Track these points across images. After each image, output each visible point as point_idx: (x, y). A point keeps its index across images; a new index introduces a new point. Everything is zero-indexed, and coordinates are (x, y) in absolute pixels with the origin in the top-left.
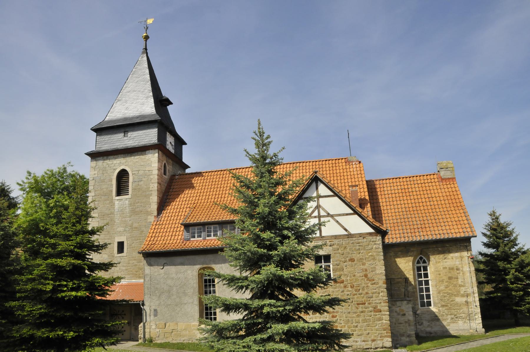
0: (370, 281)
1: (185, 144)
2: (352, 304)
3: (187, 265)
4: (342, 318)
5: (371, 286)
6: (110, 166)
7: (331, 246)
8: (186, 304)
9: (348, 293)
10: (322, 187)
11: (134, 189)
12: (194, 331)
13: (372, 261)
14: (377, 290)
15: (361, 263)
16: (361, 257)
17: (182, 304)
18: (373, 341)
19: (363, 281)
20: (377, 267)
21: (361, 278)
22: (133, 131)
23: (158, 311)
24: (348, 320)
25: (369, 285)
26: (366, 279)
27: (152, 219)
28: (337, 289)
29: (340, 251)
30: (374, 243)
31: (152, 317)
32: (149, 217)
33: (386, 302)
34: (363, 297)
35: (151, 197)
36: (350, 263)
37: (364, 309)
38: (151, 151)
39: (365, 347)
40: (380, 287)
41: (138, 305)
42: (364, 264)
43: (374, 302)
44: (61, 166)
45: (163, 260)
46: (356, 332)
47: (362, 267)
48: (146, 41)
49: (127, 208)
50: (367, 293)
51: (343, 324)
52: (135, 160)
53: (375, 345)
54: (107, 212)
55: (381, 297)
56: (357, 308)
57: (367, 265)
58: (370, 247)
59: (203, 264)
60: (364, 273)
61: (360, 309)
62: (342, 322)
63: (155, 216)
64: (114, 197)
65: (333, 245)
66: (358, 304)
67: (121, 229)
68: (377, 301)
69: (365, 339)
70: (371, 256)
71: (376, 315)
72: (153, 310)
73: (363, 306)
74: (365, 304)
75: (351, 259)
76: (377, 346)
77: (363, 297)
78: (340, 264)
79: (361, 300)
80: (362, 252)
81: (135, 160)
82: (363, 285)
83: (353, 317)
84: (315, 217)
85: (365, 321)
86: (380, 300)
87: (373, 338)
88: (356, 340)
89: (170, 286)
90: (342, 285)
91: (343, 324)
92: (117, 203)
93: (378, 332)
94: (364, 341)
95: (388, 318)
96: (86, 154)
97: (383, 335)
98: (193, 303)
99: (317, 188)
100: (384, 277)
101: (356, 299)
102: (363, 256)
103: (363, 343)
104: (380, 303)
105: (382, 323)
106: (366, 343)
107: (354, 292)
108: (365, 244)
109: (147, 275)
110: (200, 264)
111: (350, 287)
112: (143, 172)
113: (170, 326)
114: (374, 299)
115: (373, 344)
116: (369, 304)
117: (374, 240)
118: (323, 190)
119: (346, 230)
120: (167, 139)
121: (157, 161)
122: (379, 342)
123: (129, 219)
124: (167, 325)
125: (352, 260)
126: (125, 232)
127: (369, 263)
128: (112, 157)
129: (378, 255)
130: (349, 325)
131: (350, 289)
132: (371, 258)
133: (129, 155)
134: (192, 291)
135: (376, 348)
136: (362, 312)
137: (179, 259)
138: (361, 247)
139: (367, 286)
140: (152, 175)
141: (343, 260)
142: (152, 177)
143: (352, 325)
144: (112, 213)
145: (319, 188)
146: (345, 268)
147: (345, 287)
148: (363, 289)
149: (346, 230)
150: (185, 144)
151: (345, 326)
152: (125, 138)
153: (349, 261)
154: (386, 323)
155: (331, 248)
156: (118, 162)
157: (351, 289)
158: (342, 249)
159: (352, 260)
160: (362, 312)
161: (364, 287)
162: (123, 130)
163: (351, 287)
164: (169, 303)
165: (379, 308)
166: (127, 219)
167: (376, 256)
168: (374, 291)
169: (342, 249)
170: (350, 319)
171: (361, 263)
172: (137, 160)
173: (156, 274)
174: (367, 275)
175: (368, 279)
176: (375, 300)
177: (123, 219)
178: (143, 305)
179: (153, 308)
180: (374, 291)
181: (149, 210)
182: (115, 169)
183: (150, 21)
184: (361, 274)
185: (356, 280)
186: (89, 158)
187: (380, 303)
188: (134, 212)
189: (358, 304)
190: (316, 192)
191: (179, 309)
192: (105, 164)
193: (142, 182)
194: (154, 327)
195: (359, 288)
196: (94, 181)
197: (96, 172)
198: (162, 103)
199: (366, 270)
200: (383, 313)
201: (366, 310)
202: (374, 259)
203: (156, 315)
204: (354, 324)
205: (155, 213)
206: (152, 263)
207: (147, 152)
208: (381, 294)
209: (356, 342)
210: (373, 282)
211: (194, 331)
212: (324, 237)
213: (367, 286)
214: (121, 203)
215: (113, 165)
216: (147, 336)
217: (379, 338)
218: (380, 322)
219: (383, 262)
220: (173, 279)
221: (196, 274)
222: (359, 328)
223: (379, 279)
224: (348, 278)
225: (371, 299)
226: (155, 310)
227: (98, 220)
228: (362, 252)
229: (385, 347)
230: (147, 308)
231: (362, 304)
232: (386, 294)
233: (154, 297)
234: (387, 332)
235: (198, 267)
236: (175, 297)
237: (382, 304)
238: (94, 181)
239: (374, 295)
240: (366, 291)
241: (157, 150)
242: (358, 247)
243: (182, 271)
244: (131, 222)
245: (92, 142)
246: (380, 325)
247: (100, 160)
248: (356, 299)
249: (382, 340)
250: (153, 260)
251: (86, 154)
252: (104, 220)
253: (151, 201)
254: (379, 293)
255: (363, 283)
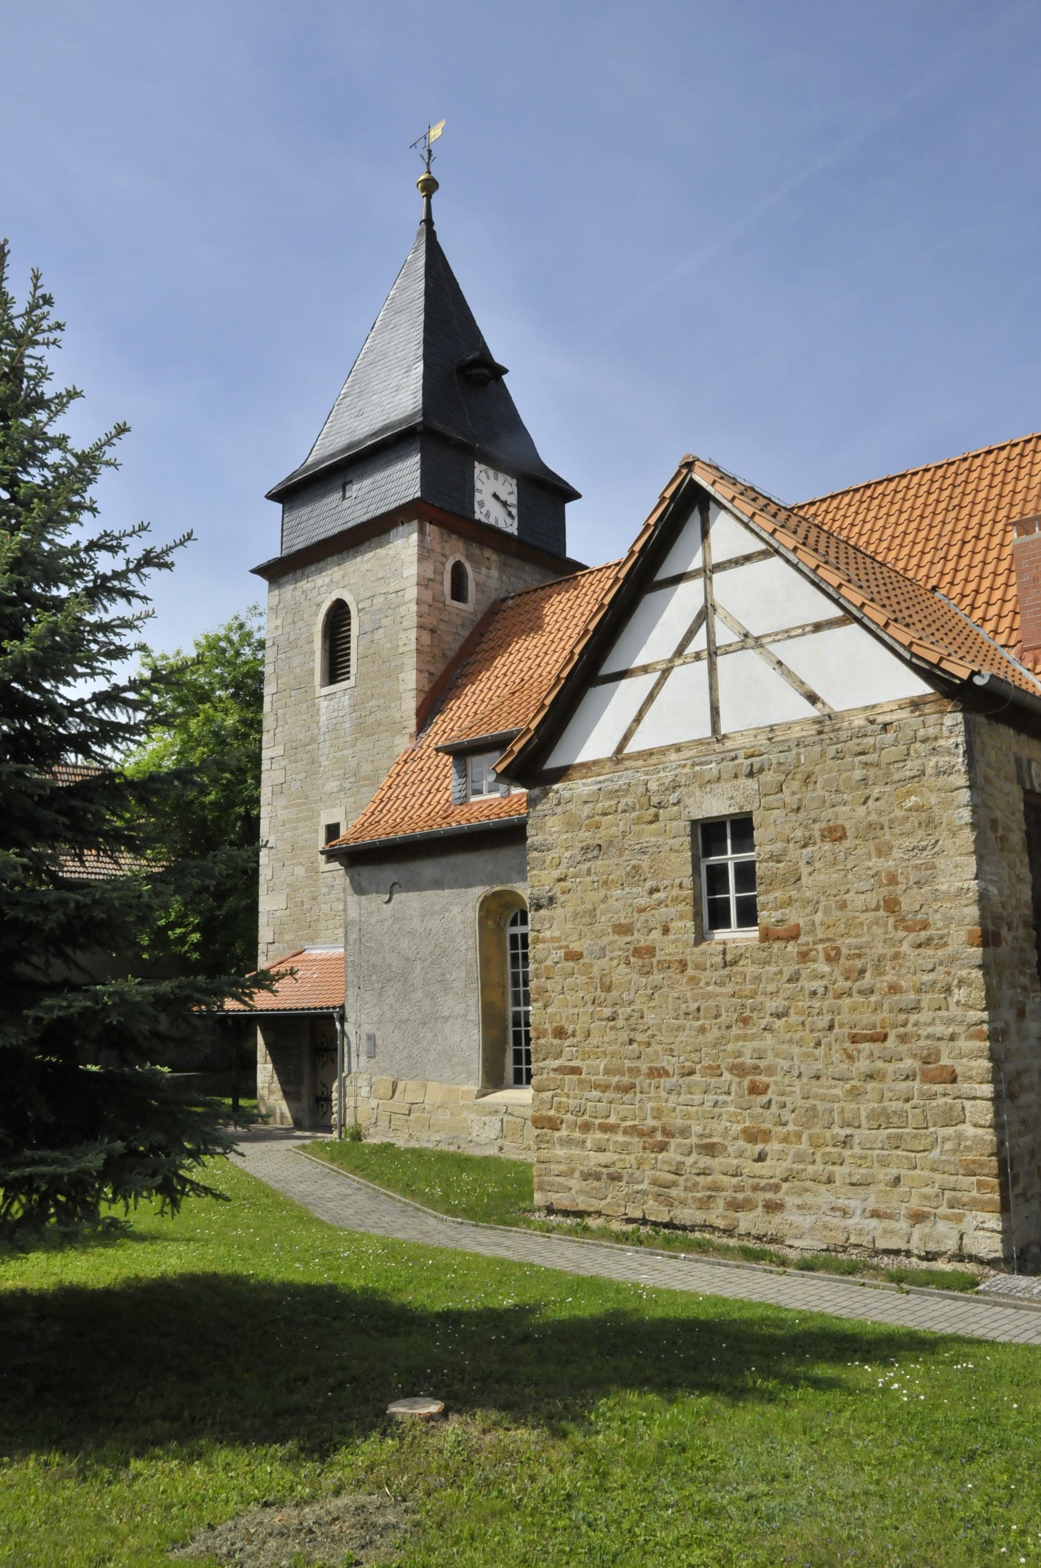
0: (908, 929)
1: (574, 495)
2: (832, 1037)
3: (450, 887)
4: (787, 1099)
5: (912, 953)
6: (311, 595)
7: (751, 774)
8: (446, 1019)
9: (816, 985)
10: (722, 525)
11: (361, 658)
12: (465, 1114)
13: (921, 833)
14: (939, 976)
15: (871, 845)
16: (873, 817)
17: (436, 1020)
18: (918, 1217)
19: (877, 930)
20: (941, 863)
21: (870, 915)
22: (362, 477)
23: (379, 1042)
24: (814, 1108)
25: (905, 948)
26: (891, 921)
27: (403, 743)
28: (772, 969)
29: (786, 795)
30: (928, 746)
31: (363, 1058)
32: (398, 740)
33: (978, 1036)
34: (878, 1007)
35: (401, 676)
36: (827, 846)
37: (880, 1064)
38: (400, 529)
39: (881, 1244)
40: (953, 959)
41: (329, 1017)
42: (883, 851)
43: (923, 1032)
44: (228, 619)
45: (389, 873)
46: (845, 1169)
47: (876, 863)
48: (429, 197)
49: (347, 718)
50: (894, 989)
51: (791, 1127)
52: (364, 567)
53: (924, 1239)
54: (301, 736)
55: (955, 1011)
56: (850, 1057)
57: (897, 854)
58: (912, 766)
59: (491, 882)
60: (884, 891)
61: (863, 1065)
62: (786, 1115)
63: (411, 736)
64: (318, 688)
65: (761, 770)
66: (854, 1039)
67: (333, 785)
68: (939, 1029)
69: (882, 1207)
70: (917, 808)
71: (933, 1096)
72: (364, 1037)
73: (875, 1047)
74: (885, 1037)
75: (831, 830)
76: (932, 1247)
77: (878, 1007)
78: (784, 852)
79: (866, 1019)
80: (876, 791)
81: (364, 567)
82: (880, 949)
83: (835, 1099)
84: (697, 657)
85: (881, 1119)
86: (950, 1021)
87: (915, 1203)
88: (841, 1203)
89: (408, 959)
90: (792, 948)
91: (791, 1127)
92: (323, 704)
93: (938, 1176)
94: (875, 1214)
95: (984, 1112)
96: (252, 571)
97: (965, 1197)
98: (465, 1015)
99: (705, 534)
100: (974, 911)
101: (844, 1017)
102: (880, 813)
103: (874, 1222)
104: (953, 1038)
105: (960, 1137)
106: (887, 1223)
107: (842, 984)
108: (889, 754)
109: (353, 922)
110: (483, 883)
111: (821, 956)
112: (381, 599)
113: (409, 1091)
114: (924, 1016)
115: (917, 1232)
116: (903, 1038)
117: (931, 731)
118: (727, 535)
119: (813, 698)
120: (478, 485)
121: (415, 558)
122: (942, 1227)
123: (350, 751)
124: (401, 1086)
125: (835, 834)
126: (341, 795)
127: (907, 843)
128: (313, 568)
129: (946, 804)
130: (816, 1130)
131: (825, 968)
132: (915, 818)
133: (351, 553)
134: (463, 975)
135: (930, 1257)
136: (870, 1077)
137: (428, 868)
138: (871, 772)
139: (896, 956)
140: (404, 604)
141: (799, 834)
142: (403, 610)
143: (828, 1134)
144: (313, 740)
145: (714, 530)
146: (805, 871)
147: (804, 956)
148: (879, 972)
149: (813, 698)
150: (574, 495)
151: (799, 1136)
152: (346, 504)
153: (823, 837)
154: (978, 1140)
155: (752, 784)
156: (327, 580)
157: (826, 969)
158: (795, 785)
159: (835, 834)
160: (870, 1077)
161: (881, 958)
162: (340, 482)
163: (829, 959)
164: (405, 1017)
165: (945, 1061)
166: (346, 752)
167: (937, 811)
168: (927, 978)
169: (795, 785)
170: (821, 1106)
171: (871, 845)
172: (369, 566)
173: (373, 921)
174: (897, 902)
175: (902, 923)
176: (929, 1023)
177: (339, 754)
178: (343, 1019)
179: (366, 1028)
180: (927, 978)
181: (397, 716)
182: (319, 605)
183: (436, 132)
184: (872, 899)
185: (849, 925)
186: (263, 583)
187: (953, 1038)
188: (362, 729)
189: (854, 1039)
190: (700, 552)
191: (429, 1036)
192: (298, 593)
193: (381, 631)
194: (364, 1092)
195: (858, 964)
196: (275, 648)
197: (279, 622)
198: (463, 375)
199: (893, 880)
200: (964, 1087)
201: (890, 1068)
202: (930, 824)
203: (371, 1056)
204: (836, 1130)
205: (412, 728)
206: (365, 884)
207: (393, 533)
208: (959, 994)
209: (845, 1213)
210: (924, 935)
211: (465, 1114)
212: (725, 736)
213: (896, 956)
214: (334, 702)
215: (315, 593)
216: (350, 1121)
217: (944, 1210)
218: (950, 1131)
219: (968, 837)
220: (412, 934)
221: (473, 915)
222: (857, 1150)
223: (949, 920)
224: (819, 917)
225: (913, 1018)
226: (371, 1038)
227: (284, 763)
228: (876, 791)
229: (972, 1258)
230: (353, 1032)
231: (873, 1039)
232: (979, 995)
233: (367, 996)
234: (980, 1185)
235: (479, 892)
236: (419, 995)
237: (964, 1044)
238: (275, 648)
239: (926, 999)
240: (889, 977)
241: (415, 524)
242: (858, 774)
243: (437, 908)
244: (354, 763)
245: (269, 534)
246: (948, 1146)
247: (287, 582)
248: (844, 1017)
249: (959, 1218)
250: (367, 873)
251: (252, 571)
252: (296, 762)
253: (402, 687)
254: (948, 990)
255: (877, 936)
